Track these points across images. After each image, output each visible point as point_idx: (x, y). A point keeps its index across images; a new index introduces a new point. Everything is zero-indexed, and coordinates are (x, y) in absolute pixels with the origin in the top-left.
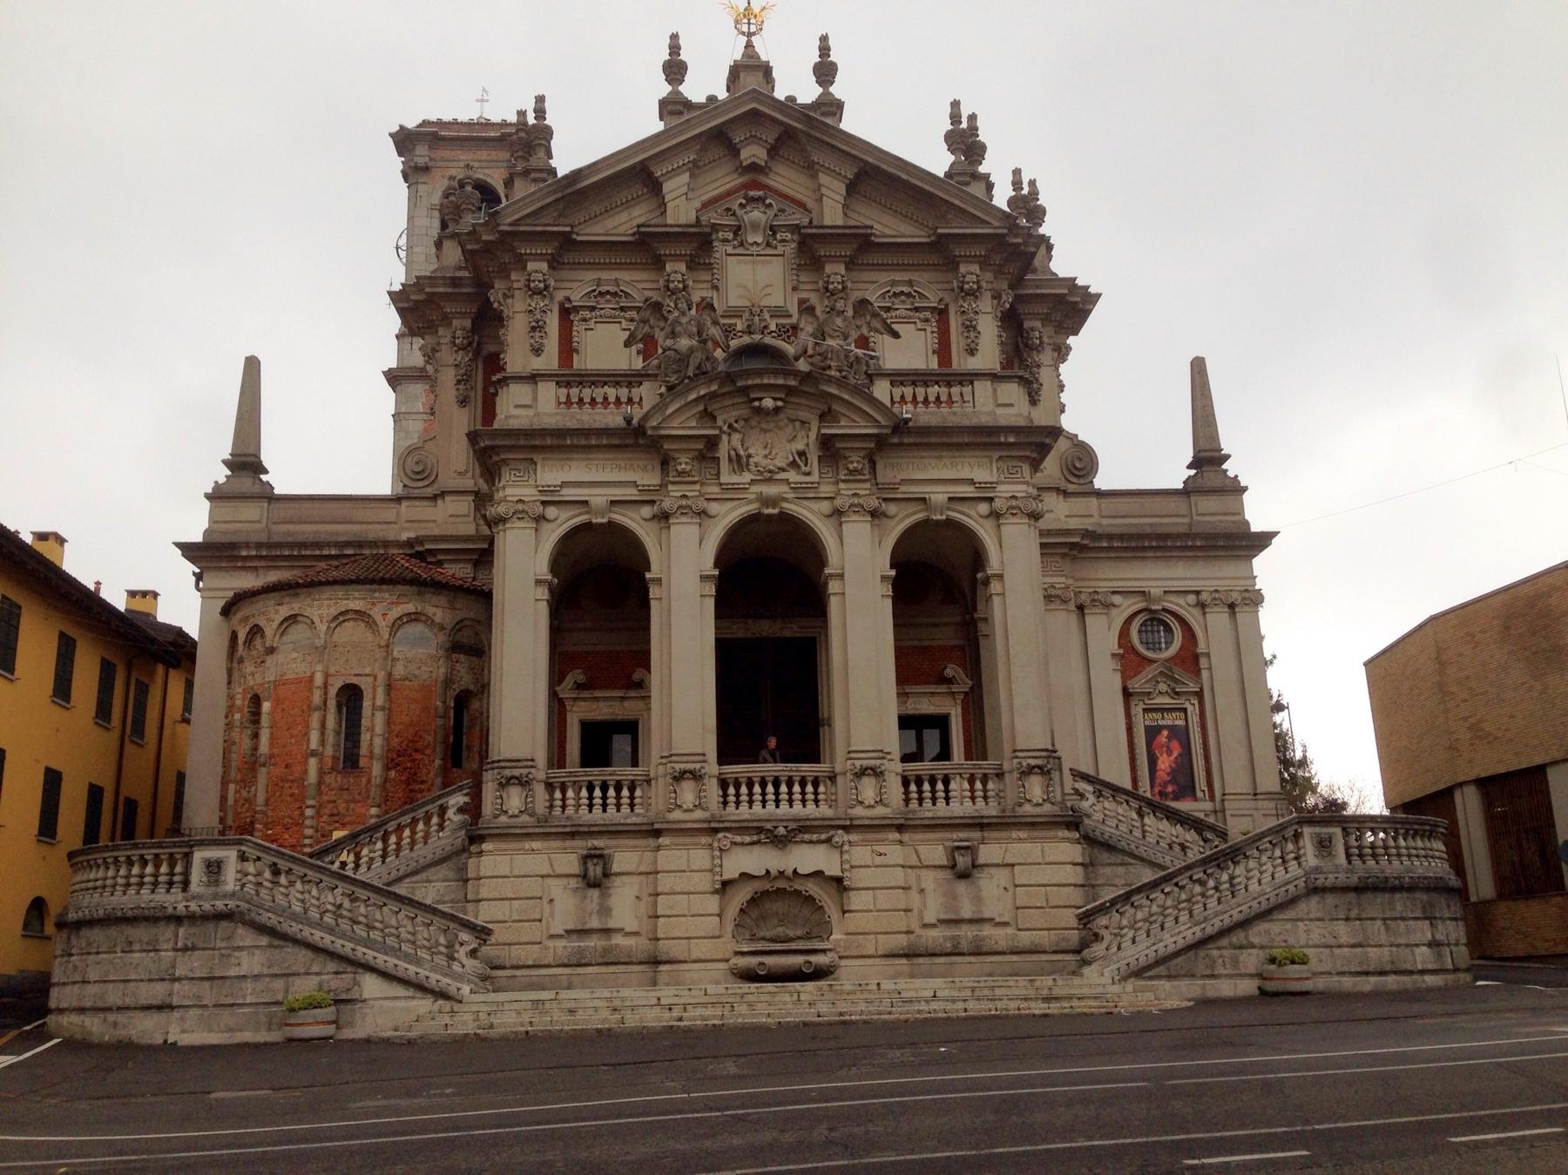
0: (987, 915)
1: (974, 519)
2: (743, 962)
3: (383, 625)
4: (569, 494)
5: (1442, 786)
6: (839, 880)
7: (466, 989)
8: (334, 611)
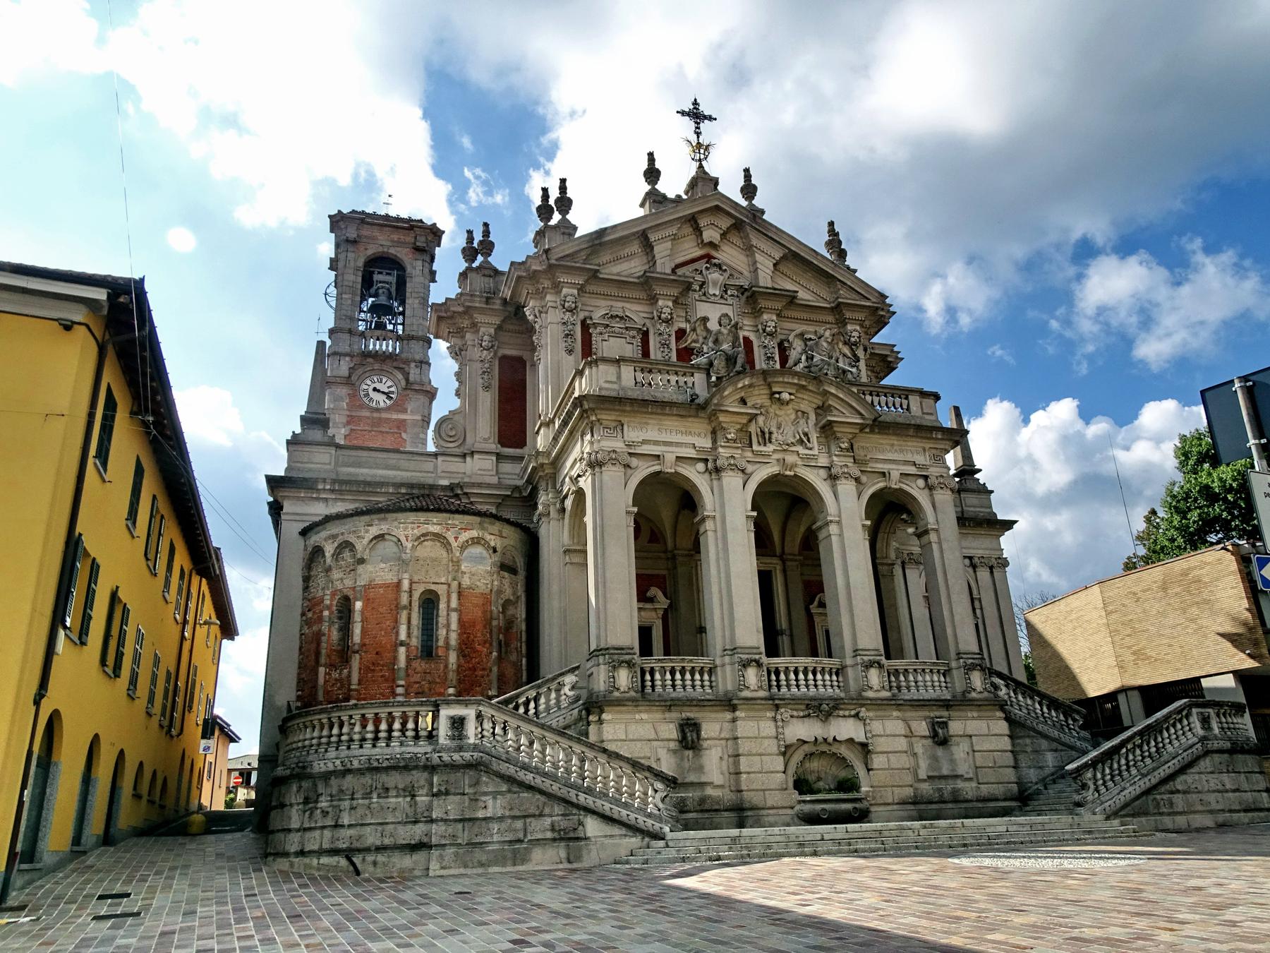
2: (807, 808)
6: (864, 746)
7: (667, 829)
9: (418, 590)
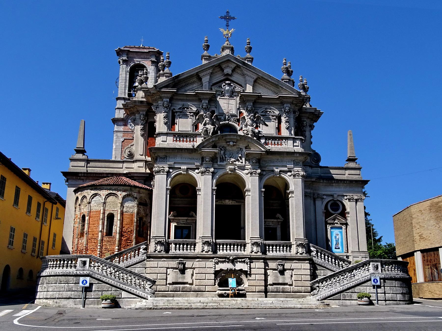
0: (286, 282)
2: (220, 292)
3: (120, 197)
5: (433, 246)
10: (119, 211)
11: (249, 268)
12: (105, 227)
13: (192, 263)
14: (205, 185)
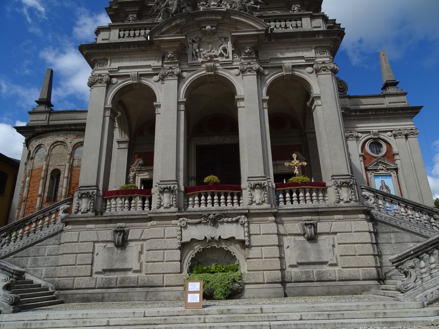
0: (325, 260)
1: (306, 74)
3: (70, 146)
4: (122, 72)
8: (52, 142)
9: (51, 169)
10: (68, 165)
11: (246, 234)
12: (47, 190)
13: (140, 231)
14: (169, 98)
